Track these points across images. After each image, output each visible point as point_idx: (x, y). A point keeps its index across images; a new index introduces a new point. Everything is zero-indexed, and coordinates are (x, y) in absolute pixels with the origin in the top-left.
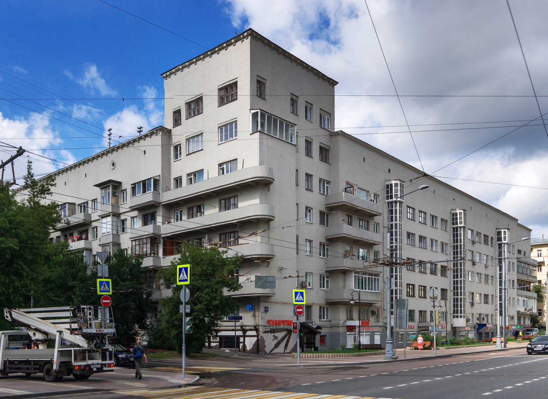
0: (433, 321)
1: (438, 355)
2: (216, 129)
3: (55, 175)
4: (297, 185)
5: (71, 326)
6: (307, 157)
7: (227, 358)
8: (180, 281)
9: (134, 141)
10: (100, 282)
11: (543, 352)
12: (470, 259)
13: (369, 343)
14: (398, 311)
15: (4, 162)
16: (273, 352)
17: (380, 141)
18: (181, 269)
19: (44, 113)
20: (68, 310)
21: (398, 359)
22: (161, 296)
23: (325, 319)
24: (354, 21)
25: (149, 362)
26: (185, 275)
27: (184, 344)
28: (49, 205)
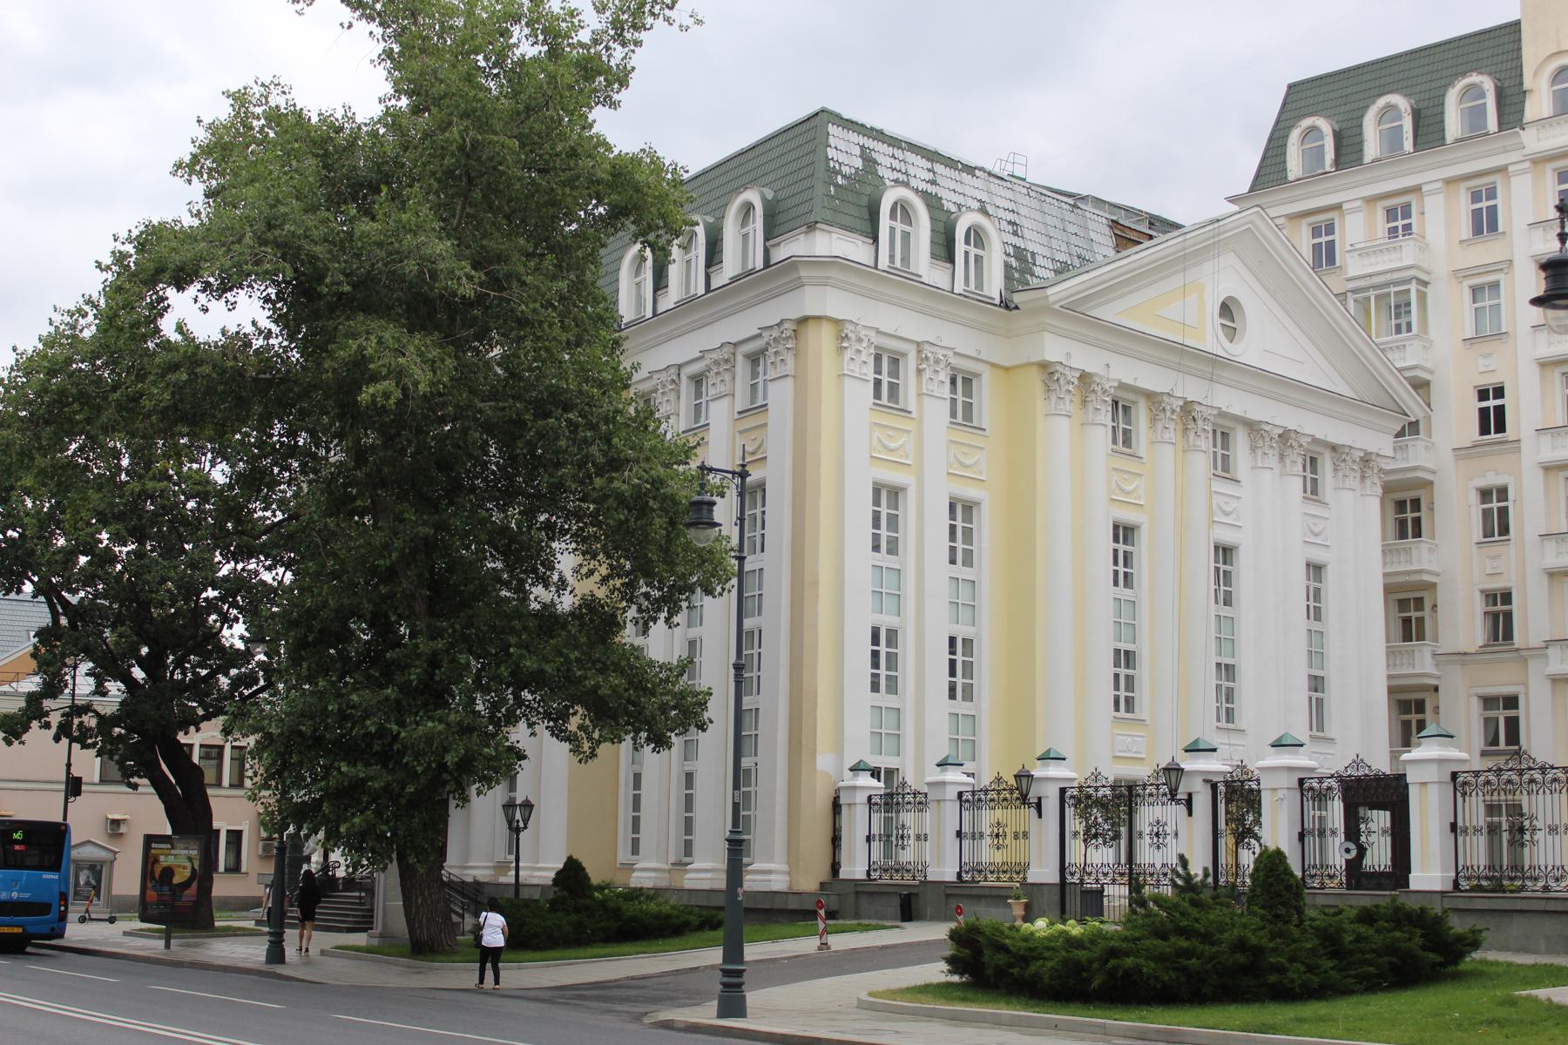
5: (824, 946)
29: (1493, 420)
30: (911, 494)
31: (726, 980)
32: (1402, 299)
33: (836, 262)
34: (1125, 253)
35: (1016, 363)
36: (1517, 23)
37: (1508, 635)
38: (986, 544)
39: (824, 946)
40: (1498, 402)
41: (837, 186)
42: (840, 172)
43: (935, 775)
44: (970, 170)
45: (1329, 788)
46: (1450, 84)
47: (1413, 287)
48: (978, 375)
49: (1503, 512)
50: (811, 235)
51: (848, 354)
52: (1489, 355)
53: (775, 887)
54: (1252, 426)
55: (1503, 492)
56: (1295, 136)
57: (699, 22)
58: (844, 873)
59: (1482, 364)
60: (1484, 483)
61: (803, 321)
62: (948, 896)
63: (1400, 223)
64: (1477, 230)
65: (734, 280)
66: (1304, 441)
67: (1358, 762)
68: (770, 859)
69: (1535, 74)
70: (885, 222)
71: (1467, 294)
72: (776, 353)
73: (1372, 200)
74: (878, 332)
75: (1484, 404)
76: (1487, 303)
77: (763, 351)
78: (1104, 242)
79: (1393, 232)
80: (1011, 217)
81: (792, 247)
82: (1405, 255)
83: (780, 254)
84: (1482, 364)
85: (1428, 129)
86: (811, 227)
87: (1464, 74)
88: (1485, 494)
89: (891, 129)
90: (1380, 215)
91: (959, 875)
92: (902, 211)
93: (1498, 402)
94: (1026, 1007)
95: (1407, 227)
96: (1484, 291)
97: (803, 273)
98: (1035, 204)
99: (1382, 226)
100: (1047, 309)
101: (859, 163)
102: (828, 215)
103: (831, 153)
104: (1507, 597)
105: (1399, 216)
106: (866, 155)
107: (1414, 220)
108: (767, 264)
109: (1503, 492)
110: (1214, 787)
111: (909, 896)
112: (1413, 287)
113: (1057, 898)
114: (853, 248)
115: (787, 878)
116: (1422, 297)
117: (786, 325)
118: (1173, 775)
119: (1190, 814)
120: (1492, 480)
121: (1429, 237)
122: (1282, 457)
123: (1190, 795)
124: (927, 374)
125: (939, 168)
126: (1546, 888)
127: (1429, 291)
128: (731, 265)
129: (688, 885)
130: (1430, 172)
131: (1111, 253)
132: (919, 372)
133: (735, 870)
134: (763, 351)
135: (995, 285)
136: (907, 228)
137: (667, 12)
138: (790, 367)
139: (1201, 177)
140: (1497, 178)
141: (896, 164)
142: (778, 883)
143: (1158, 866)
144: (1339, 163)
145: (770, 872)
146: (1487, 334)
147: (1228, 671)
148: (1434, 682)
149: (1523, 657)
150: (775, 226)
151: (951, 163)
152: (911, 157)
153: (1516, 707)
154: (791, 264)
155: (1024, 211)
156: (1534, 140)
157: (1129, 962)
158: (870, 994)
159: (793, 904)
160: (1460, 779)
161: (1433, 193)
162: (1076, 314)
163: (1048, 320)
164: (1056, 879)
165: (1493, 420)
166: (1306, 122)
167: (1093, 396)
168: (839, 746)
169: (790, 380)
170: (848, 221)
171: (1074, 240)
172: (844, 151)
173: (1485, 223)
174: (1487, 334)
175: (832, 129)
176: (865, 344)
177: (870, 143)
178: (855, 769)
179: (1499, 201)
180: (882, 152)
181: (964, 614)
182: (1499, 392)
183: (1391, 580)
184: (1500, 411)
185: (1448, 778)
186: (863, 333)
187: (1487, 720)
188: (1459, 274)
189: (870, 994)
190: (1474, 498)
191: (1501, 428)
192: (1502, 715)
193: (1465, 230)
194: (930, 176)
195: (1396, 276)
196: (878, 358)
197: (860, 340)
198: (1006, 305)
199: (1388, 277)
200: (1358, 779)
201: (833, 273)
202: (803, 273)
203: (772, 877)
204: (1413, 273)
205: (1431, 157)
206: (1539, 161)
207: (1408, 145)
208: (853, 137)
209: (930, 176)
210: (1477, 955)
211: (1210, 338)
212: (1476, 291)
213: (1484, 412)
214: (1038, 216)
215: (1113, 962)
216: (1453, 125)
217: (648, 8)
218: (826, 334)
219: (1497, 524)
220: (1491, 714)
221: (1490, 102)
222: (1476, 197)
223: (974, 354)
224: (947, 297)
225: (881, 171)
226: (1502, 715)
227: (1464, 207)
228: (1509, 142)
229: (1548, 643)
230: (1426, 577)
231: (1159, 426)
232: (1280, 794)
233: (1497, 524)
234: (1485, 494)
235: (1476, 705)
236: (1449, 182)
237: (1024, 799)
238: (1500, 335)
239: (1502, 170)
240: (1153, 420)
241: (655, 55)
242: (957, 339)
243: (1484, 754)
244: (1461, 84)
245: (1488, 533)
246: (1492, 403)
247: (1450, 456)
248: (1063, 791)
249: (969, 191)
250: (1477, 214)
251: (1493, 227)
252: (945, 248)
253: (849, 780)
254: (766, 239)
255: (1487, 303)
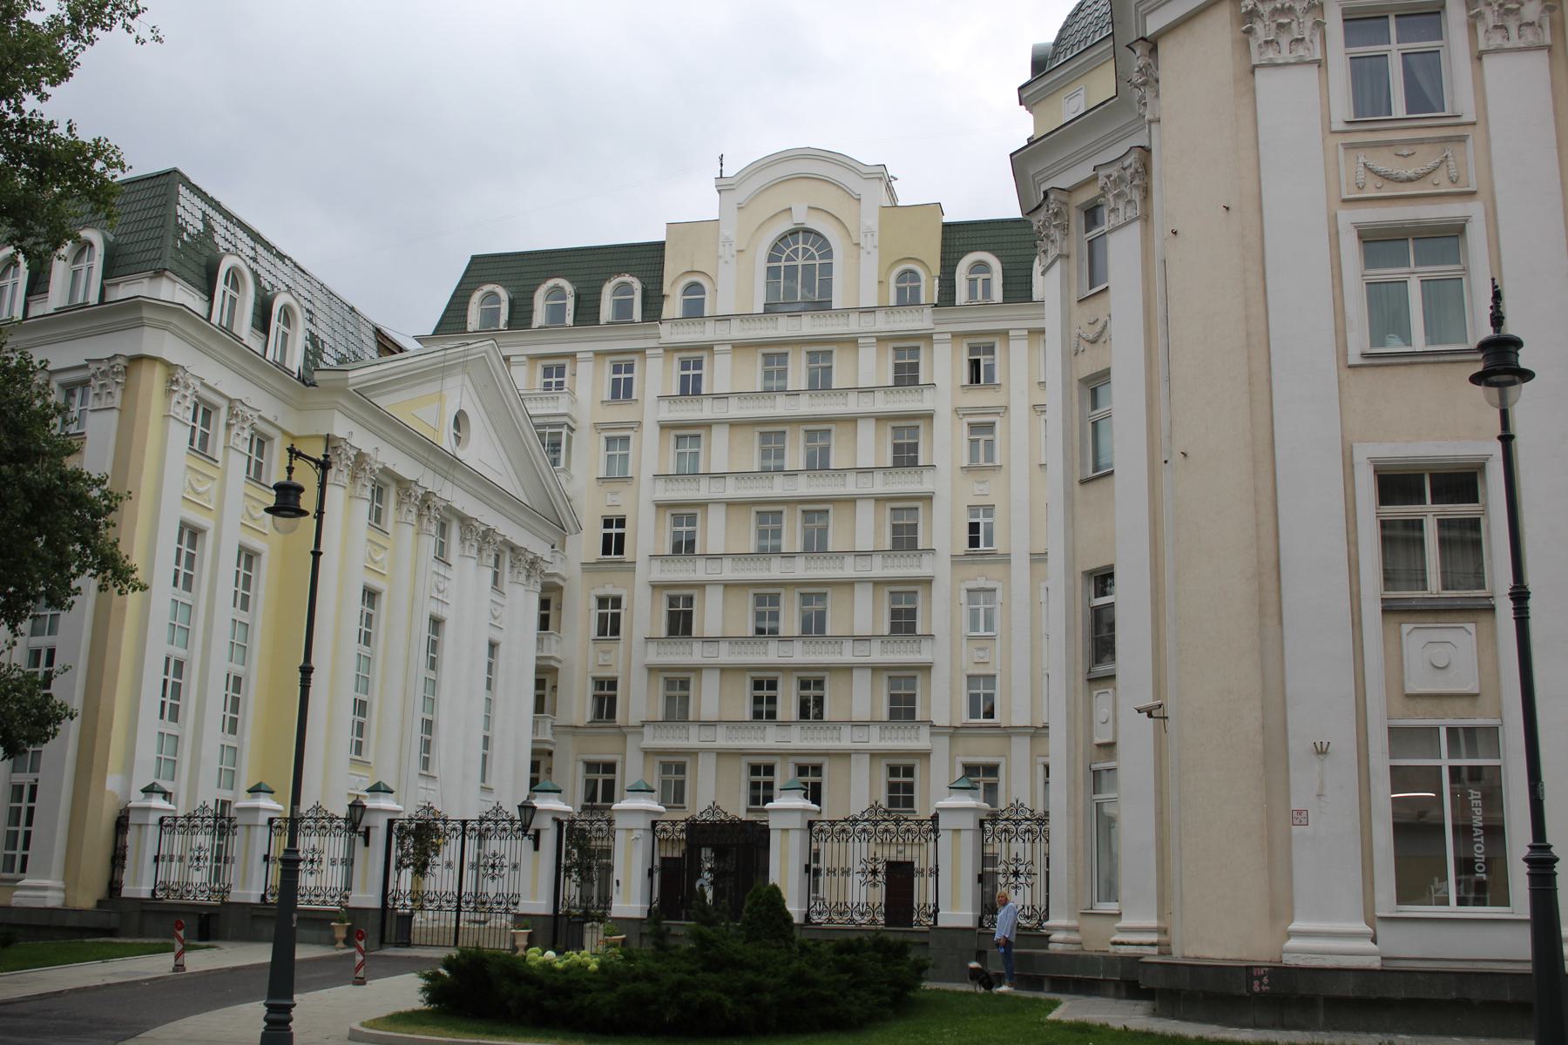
1: (218, 388)
4: (436, 623)
5: (179, 967)
7: (1499, 701)
10: (1418, 525)
13: (270, 946)
14: (931, 901)
15: (894, 183)
17: (1292, 744)
19: (94, 459)
21: (1463, 120)
22: (302, 942)
29: (613, 544)
30: (210, 538)
31: (273, 1016)
32: (555, 439)
33: (179, 310)
34: (385, 359)
35: (304, 433)
36: (663, 244)
37: (611, 714)
38: (261, 592)
39: (179, 967)
40: (620, 530)
41: (183, 241)
42: (185, 230)
43: (245, 801)
44: (281, 257)
45: (488, 829)
46: (607, 279)
47: (565, 431)
48: (270, 439)
49: (616, 617)
50: (156, 281)
51: (176, 397)
52: (616, 493)
53: (50, 904)
54: (465, 521)
55: (617, 602)
56: (476, 297)
57: (159, 40)
58: (128, 890)
59: (610, 499)
60: (602, 592)
61: (138, 359)
62: (254, 917)
63: (554, 380)
64: (615, 395)
65: (59, 311)
66: (499, 539)
67: (714, 808)
68: (47, 876)
69: (673, 284)
70: (220, 285)
71: (603, 443)
72: (102, 386)
73: (534, 358)
74: (203, 384)
75: (608, 531)
76: (618, 452)
77: (85, 384)
78: (371, 349)
79: (548, 385)
80: (309, 306)
81: (121, 292)
82: (557, 406)
83: (121, 292)
84: (610, 499)
85: (587, 312)
86: (159, 273)
87: (619, 274)
88: (602, 602)
89: (226, 204)
90: (539, 372)
91: (154, 892)
92: (234, 278)
93: (620, 530)
94: (469, 1031)
95: (560, 385)
96: (617, 441)
97: (146, 314)
98: (325, 299)
99: (539, 379)
100: (342, 390)
101: (200, 226)
102: (175, 265)
103: (180, 211)
104: (613, 684)
105: (555, 372)
106: (206, 219)
107: (567, 379)
108: (102, 300)
109: (617, 602)
110: (560, 824)
111: (208, 916)
112: (565, 431)
113: (378, 921)
114: (193, 300)
115: (62, 895)
116: (569, 439)
117: (119, 360)
118: (529, 812)
119: (536, 848)
120: (609, 591)
121: (578, 394)
122: (480, 550)
123: (368, 829)
124: (234, 430)
125: (260, 249)
126: (830, 920)
127: (574, 435)
128: (57, 296)
129: (14, 902)
130: (584, 344)
131: (375, 355)
132: (229, 426)
133: (989, 906)
134: (85, 384)
135: (295, 362)
136: (234, 294)
137: (128, 20)
138: (117, 401)
139: (413, 312)
140: (635, 357)
141: (228, 235)
142: (53, 900)
143: (492, 895)
144: (511, 324)
145: (45, 888)
146: (616, 476)
147: (428, 726)
148: (548, 747)
149: (623, 732)
150: (115, 267)
151: (269, 247)
152: (240, 233)
153: (614, 772)
154: (135, 304)
155: (318, 304)
156: (669, 334)
157: (705, 993)
158: (363, 1024)
159: (72, 921)
160: (659, 827)
161: (519, 364)
162: (362, 398)
163: (342, 401)
164: (550, 911)
165: (613, 544)
166: (488, 288)
167: (362, 474)
168: (128, 768)
169: (115, 413)
170: (189, 275)
171: (351, 338)
172: (189, 211)
173: (622, 390)
174: (616, 476)
175: (182, 189)
176: (190, 391)
177: (210, 211)
178: (149, 790)
179: (636, 375)
180: (218, 220)
181: (237, 652)
182: (621, 523)
183: (543, 663)
184: (620, 537)
185: (805, 826)
186: (191, 381)
187: (588, 781)
188: (599, 427)
189: (363, 1024)
190: (594, 603)
191: (620, 551)
192: (601, 778)
193: (606, 393)
194: (252, 254)
195: (551, 420)
196: (196, 406)
197: (187, 387)
198: (306, 381)
199: (546, 420)
200: (713, 824)
201: (175, 320)
202: (146, 314)
203: (48, 893)
204: (566, 419)
205: (588, 332)
206: (670, 350)
207: (569, 320)
208: (197, 201)
209: (252, 254)
210: (927, 985)
211: (446, 442)
212: (610, 441)
213: (607, 537)
214: (326, 310)
215: (685, 995)
216: (606, 311)
217: (108, 10)
218: (159, 373)
219: (610, 626)
220: (593, 776)
221: (570, 304)
222: (617, 369)
223: (271, 419)
224: (257, 359)
225: (217, 239)
226: (601, 778)
227: (607, 375)
228: (649, 331)
229: (644, 724)
230: (553, 663)
231: (405, 508)
232: (636, 834)
233: (610, 626)
234: (602, 602)
235: (581, 769)
236: (597, 354)
237: (525, 829)
238: (626, 479)
239: (641, 352)
240: (400, 503)
241: (104, 57)
242: (261, 402)
243: (584, 808)
244: (616, 281)
245: (602, 632)
246: (614, 531)
247: (579, 567)
248: (391, 822)
249: (280, 275)
250: (616, 382)
251: (628, 394)
252: (262, 320)
253: (137, 800)
254: (104, 277)
255: (618, 452)
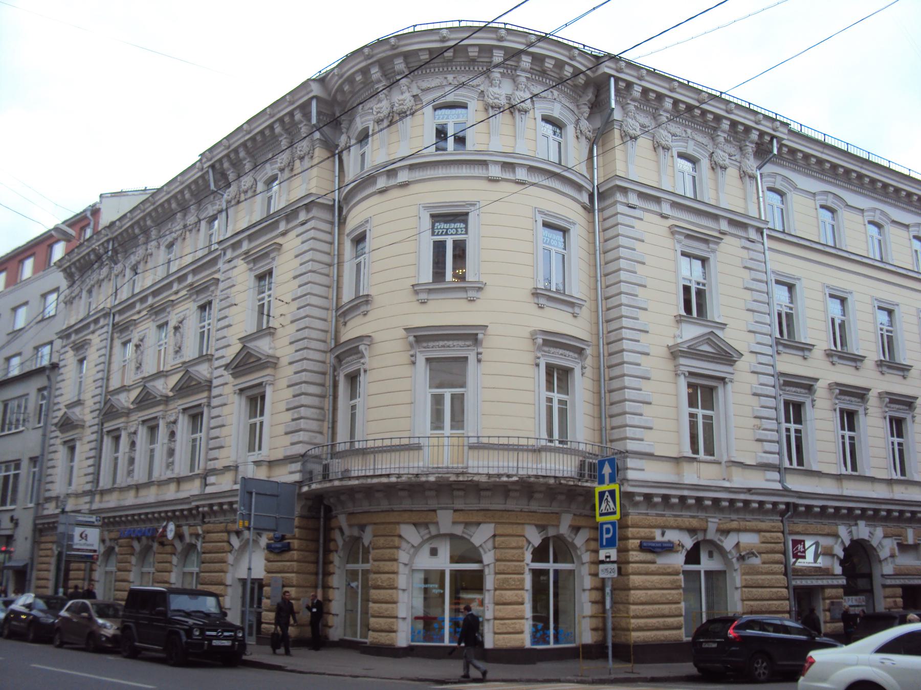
0: (288, 222)
2: (39, 297)
3: (651, 100)
6: (249, 426)
8: (601, 515)
9: (427, 63)
10: (793, 541)
11: (915, 547)
12: (197, 483)
16: (497, 21)
18: (602, 494)
20: (635, 630)
23: (795, 465)
24: (33, 455)
25: (516, 530)
26: (611, 504)
27: (104, 678)
28: (327, 626)
59: (719, 540)
109: (460, 217)
